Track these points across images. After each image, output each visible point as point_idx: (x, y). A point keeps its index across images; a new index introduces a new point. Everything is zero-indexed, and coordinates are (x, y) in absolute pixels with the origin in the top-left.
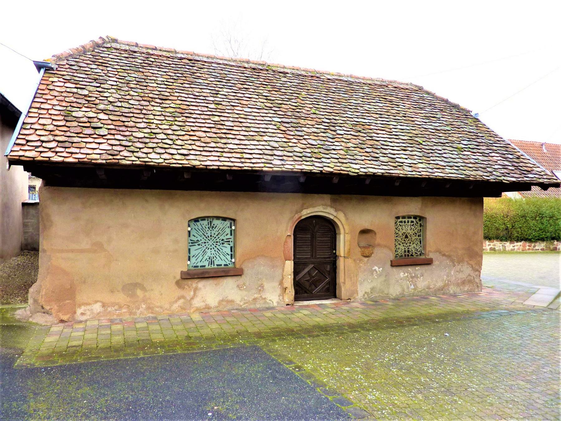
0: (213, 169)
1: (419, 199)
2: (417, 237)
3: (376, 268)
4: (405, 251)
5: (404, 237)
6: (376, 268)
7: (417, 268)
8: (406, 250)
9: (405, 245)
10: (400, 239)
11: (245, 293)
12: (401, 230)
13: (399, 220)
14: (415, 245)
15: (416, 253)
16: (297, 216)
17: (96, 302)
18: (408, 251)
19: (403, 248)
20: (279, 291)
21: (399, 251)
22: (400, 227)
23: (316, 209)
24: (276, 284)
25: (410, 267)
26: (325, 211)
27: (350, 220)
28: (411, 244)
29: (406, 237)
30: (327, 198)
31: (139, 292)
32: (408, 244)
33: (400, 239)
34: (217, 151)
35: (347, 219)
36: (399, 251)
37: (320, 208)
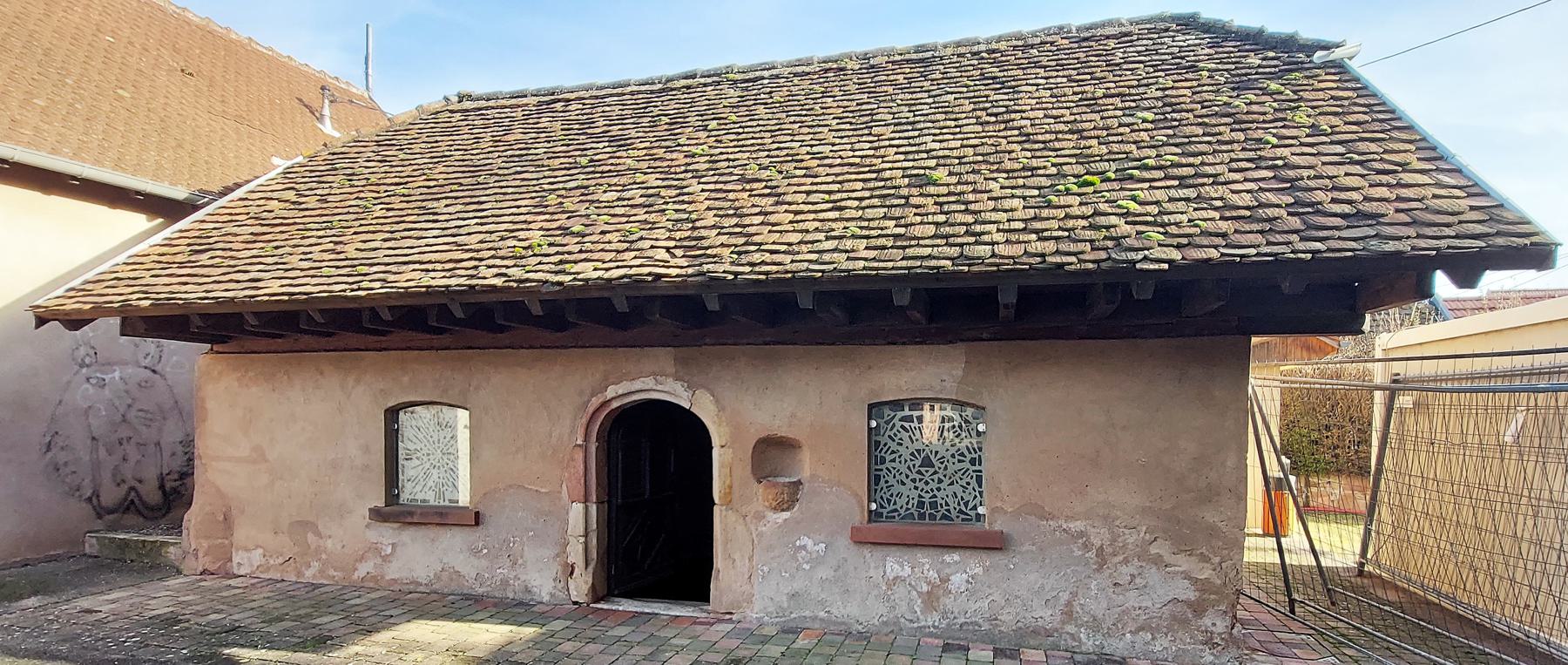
0: (980, 272)
1: (958, 351)
2: (967, 465)
3: (808, 542)
4: (921, 504)
5: (918, 463)
6: (808, 542)
7: (947, 558)
8: (927, 500)
9: (920, 485)
10: (904, 469)
11: (484, 563)
12: (907, 441)
13: (900, 414)
14: (957, 488)
15: (961, 511)
16: (595, 402)
17: (257, 547)
18: (934, 505)
19: (915, 494)
20: (556, 568)
21: (901, 502)
22: (905, 435)
23: (637, 385)
24: (548, 552)
25: (926, 551)
26: (659, 387)
27: (733, 410)
28: (942, 486)
29: (927, 463)
30: (664, 357)
31: (311, 537)
32: (934, 485)
33: (904, 469)
34: (1439, 212)
35: (721, 409)
36: (901, 502)
37: (649, 382)
